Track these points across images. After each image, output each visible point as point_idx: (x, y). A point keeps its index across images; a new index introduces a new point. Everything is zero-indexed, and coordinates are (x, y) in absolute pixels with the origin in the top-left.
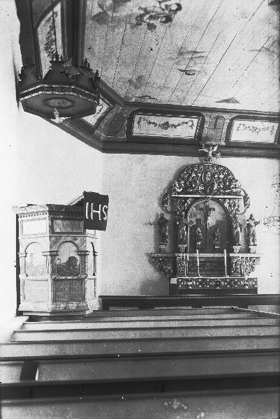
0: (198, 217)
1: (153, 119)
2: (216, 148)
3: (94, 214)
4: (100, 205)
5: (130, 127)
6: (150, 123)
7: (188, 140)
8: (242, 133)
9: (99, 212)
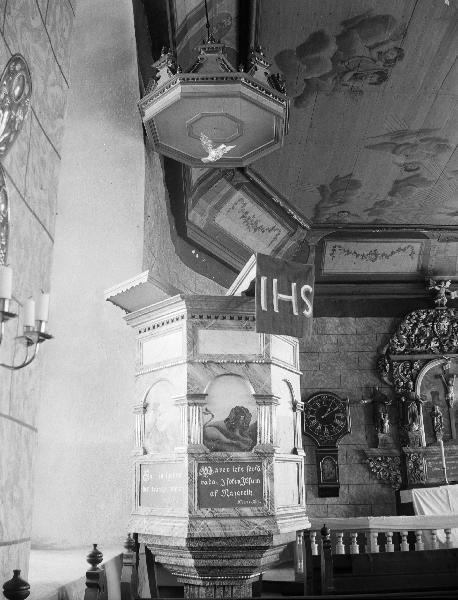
0: (434, 389)
1: (352, 246)
2: (448, 284)
3: (280, 302)
4: (294, 285)
5: (319, 262)
6: (348, 252)
7: (411, 275)
8: (12, 136)
9: (293, 298)
